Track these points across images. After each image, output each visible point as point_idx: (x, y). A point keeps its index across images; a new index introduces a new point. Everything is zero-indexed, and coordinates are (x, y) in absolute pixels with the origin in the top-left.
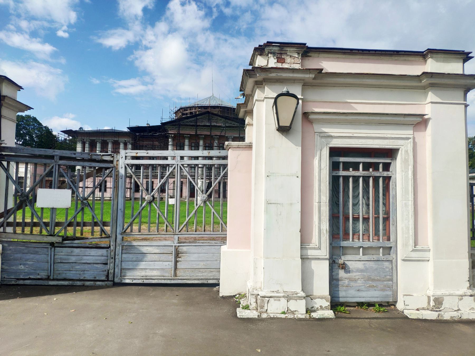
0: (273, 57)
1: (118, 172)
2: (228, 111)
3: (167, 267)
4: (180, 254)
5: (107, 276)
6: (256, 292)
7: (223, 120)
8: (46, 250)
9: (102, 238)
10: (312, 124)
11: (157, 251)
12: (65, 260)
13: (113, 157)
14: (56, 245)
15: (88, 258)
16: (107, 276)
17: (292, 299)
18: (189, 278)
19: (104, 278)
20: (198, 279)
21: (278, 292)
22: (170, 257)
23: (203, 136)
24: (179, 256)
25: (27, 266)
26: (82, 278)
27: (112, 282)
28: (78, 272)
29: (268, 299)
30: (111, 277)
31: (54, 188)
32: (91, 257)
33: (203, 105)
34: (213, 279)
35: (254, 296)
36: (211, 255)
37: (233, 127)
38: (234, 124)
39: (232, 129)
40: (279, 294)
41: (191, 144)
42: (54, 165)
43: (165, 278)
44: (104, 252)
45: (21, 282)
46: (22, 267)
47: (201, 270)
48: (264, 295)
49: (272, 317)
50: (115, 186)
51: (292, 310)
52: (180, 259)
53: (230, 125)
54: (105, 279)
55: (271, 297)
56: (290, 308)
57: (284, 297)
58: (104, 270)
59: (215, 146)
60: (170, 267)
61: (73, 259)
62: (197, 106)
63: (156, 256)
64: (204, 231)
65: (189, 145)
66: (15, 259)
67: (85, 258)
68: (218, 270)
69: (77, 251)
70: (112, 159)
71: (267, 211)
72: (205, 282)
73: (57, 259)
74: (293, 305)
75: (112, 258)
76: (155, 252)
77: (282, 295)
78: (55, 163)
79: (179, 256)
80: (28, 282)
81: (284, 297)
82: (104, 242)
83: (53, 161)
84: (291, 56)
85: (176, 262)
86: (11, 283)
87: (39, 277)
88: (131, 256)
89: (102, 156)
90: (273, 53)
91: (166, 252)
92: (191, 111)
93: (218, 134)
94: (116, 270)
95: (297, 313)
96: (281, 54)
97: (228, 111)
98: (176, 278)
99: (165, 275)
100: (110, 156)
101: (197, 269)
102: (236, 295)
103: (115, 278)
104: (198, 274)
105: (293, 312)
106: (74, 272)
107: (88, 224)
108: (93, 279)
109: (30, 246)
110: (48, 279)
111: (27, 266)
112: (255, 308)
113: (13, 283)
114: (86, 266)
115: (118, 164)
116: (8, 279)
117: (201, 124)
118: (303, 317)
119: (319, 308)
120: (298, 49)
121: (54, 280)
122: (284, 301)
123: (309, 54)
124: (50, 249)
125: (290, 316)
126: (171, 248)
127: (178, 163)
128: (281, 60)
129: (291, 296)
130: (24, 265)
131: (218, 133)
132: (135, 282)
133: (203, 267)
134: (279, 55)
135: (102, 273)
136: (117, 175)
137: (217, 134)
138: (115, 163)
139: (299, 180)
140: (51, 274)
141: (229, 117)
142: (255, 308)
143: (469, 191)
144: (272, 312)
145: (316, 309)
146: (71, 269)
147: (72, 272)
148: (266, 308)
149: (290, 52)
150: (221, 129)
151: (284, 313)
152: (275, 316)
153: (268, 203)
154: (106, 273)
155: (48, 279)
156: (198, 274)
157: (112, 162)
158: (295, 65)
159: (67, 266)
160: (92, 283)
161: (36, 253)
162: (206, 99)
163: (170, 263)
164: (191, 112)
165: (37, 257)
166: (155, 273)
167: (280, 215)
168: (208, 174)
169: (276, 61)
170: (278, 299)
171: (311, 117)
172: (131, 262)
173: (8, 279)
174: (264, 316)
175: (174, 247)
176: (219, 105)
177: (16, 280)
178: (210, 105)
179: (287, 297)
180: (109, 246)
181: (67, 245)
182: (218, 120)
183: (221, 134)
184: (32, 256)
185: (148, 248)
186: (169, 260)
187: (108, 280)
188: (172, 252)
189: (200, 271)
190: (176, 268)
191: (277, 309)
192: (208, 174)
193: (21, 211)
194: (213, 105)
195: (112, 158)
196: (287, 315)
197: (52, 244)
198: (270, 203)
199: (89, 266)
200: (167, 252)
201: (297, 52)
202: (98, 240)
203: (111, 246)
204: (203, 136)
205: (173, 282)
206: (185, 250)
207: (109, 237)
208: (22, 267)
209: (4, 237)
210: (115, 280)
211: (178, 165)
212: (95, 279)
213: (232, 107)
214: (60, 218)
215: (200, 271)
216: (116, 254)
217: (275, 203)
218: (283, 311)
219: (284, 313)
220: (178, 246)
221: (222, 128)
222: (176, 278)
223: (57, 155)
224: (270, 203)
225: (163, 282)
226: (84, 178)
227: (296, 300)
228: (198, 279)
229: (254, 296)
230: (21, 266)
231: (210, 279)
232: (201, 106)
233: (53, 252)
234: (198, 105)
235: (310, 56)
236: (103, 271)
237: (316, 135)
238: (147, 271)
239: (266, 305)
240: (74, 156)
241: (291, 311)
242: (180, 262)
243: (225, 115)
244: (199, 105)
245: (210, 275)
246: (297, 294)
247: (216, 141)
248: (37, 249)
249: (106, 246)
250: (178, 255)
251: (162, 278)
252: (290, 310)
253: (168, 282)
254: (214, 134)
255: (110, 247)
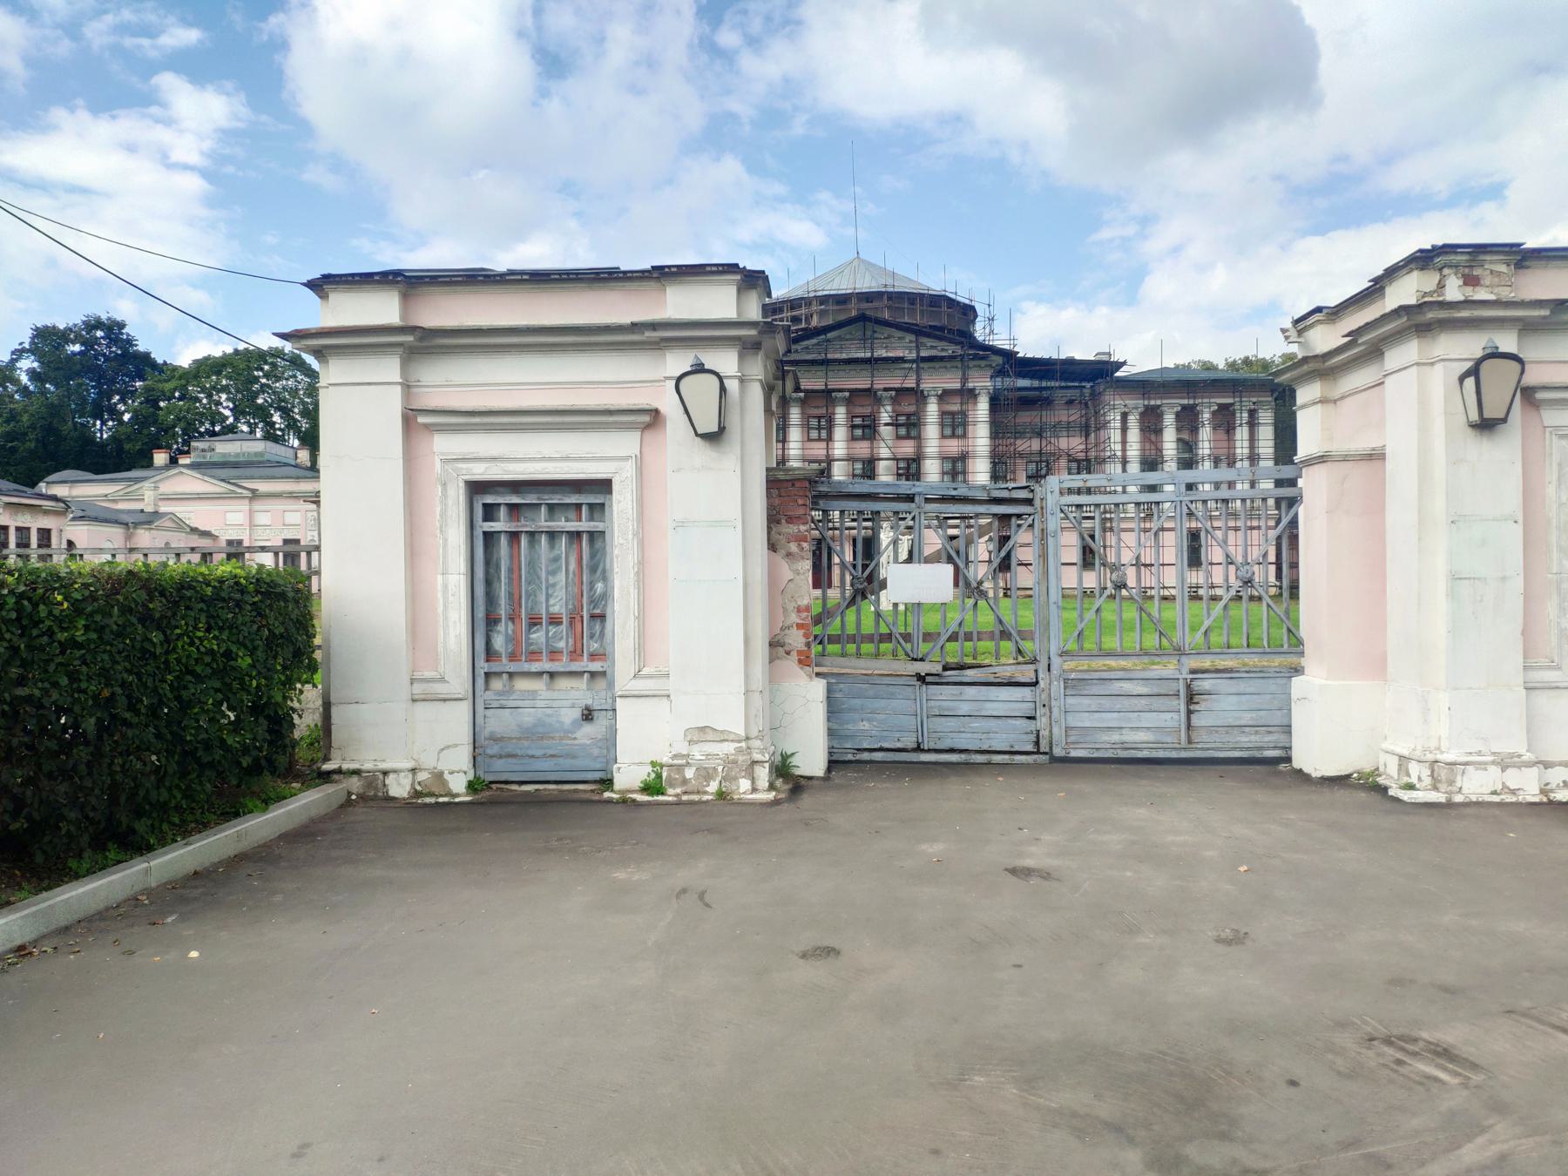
0: (1456, 274)
1: (1045, 523)
2: (912, 307)
3: (1169, 724)
4: (1197, 696)
5: (1037, 743)
6: (1430, 757)
7: (910, 337)
8: (910, 689)
9: (1019, 663)
10: (1538, 410)
11: (1145, 690)
12: (948, 710)
13: (1032, 491)
14: (929, 679)
15: (995, 705)
16: (1037, 743)
17: (1510, 766)
18: (1220, 745)
19: (1030, 748)
20: (1241, 749)
21: (1479, 753)
22: (1175, 702)
23: (847, 394)
24: (1195, 700)
25: (875, 723)
26: (985, 747)
27: (1048, 757)
28: (975, 736)
29: (1463, 767)
30: (1044, 747)
31: (919, 562)
32: (1001, 705)
33: (832, 292)
34: (1275, 748)
35: (1427, 764)
36: (1268, 696)
37: (942, 359)
38: (943, 350)
39: (937, 365)
40: (1484, 757)
41: (808, 421)
42: (917, 514)
43: (1165, 745)
44: (1026, 692)
45: (866, 756)
46: (865, 725)
47: (1247, 729)
48: (1453, 760)
49: (1474, 800)
50: (1041, 554)
51: (1512, 788)
52: (1196, 707)
53: (933, 353)
54: (1032, 750)
55: (1466, 764)
56: (1508, 784)
57: (1493, 763)
58: (1028, 730)
59: (886, 424)
60: (1176, 724)
61: (965, 708)
62: (815, 297)
63: (1143, 701)
64: (1248, 646)
65: (802, 426)
66: (851, 710)
67: (988, 705)
68: (1287, 730)
69: (971, 692)
70: (1030, 496)
71: (1452, 595)
72: (1257, 754)
73: (931, 707)
74: (1514, 778)
75: (1044, 706)
76: (1140, 693)
77: (1490, 758)
78: (918, 510)
79: (1195, 700)
80: (878, 756)
81: (1493, 763)
82: (1026, 674)
83: (913, 505)
84: (1492, 272)
85: (1189, 713)
86: (847, 759)
87: (899, 745)
88: (1086, 701)
89: (1010, 490)
90: (1456, 267)
91: (1163, 692)
92: (794, 313)
93: (896, 386)
94: (1056, 730)
95: (1521, 792)
96: (1471, 267)
97: (913, 304)
98: (1191, 746)
99: (1163, 741)
100: (1026, 490)
101: (1236, 728)
102: (1352, 774)
103: (1054, 748)
104: (1239, 738)
105: (1513, 792)
106: (969, 735)
107: (984, 636)
108: (1008, 749)
109: (878, 682)
110: (918, 749)
111: (875, 723)
112: (1429, 787)
113: (850, 757)
114: (993, 723)
115: (1044, 505)
116: (840, 751)
117: (837, 356)
118: (1537, 799)
119: (1562, 784)
120: (1509, 256)
121: (929, 751)
122: (1494, 771)
123: (1527, 263)
124: (917, 687)
125: (1510, 799)
126: (1176, 684)
127: (1181, 499)
128: (1471, 281)
129: (1509, 760)
130: (869, 720)
131: (896, 383)
132: (1096, 755)
133: (1251, 723)
134: (1467, 271)
135: (1024, 737)
136: (1043, 530)
137: (892, 386)
138: (1037, 502)
139: (1519, 529)
140: (923, 739)
141: (917, 325)
142: (1429, 787)
143: (923, 566)
144: (1471, 792)
145: (1554, 787)
146: (962, 730)
147: (963, 735)
148: (1458, 784)
149: (1491, 262)
150: (901, 369)
151: (1494, 793)
152: (1480, 799)
153: (1455, 578)
154: (1033, 737)
155: (918, 749)
156: (1239, 738)
157: (1029, 502)
158: (1501, 288)
159: (952, 723)
160: (1007, 757)
161: (891, 697)
162: (840, 270)
163: (1175, 715)
164: (794, 316)
165: (894, 703)
166: (1141, 736)
167: (1481, 601)
168: (853, 514)
169: (1461, 282)
170: (1483, 766)
171: (1540, 395)
172: (1087, 714)
173: (840, 751)
174: (1458, 799)
175: (1181, 681)
176: (883, 290)
177: (856, 752)
178: (857, 291)
179: (1499, 763)
180: (1034, 680)
181: (951, 680)
182: (893, 340)
183: (904, 385)
184: (883, 703)
185: (1122, 685)
186: (1171, 709)
187: (1038, 752)
188: (1179, 691)
189: (1244, 732)
190: (1189, 726)
191: (1481, 786)
192: (853, 514)
193: (854, 608)
194: (864, 291)
195: (1031, 494)
196: (1502, 797)
197: (921, 678)
198: (1460, 579)
199: (999, 722)
200: (1166, 693)
201: (1505, 263)
202: (1013, 667)
203: (1040, 679)
204: (847, 394)
205: (1184, 755)
206: (1207, 687)
207: (1034, 661)
208: (865, 725)
209: (828, 664)
210: (1054, 752)
211: (1181, 501)
212: (1012, 750)
213: (926, 292)
214: (931, 622)
215: (1244, 732)
216: (1052, 696)
217: (1470, 578)
218: (1493, 789)
219: (1494, 793)
220: (1192, 680)
221: (907, 365)
222: (1191, 746)
223: (920, 494)
224: (1460, 579)
225: (1161, 754)
226: (976, 537)
227: (1519, 767)
228: (1241, 749)
229: (1427, 764)
230: (864, 723)
231: (1269, 748)
232: (826, 295)
233: (924, 695)
234: (815, 291)
235: (1527, 267)
236: (1027, 733)
237: (1547, 434)
238: (1124, 731)
239: (1459, 778)
240: (873, 490)
241: (1511, 790)
242: (1196, 713)
243: (903, 321)
244: (820, 294)
245: (1266, 739)
246: (1520, 756)
247: (889, 408)
248: (891, 689)
249: (1028, 680)
250: (1191, 699)
251: (1160, 745)
252: (1508, 788)
253: (1174, 755)
254: (881, 386)
255: (1037, 682)
